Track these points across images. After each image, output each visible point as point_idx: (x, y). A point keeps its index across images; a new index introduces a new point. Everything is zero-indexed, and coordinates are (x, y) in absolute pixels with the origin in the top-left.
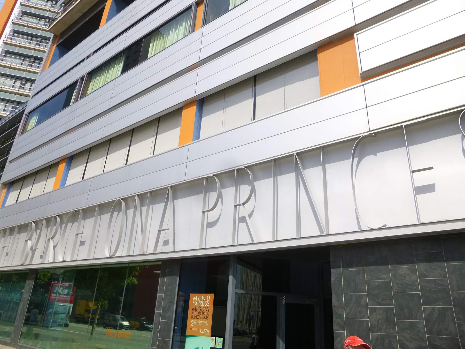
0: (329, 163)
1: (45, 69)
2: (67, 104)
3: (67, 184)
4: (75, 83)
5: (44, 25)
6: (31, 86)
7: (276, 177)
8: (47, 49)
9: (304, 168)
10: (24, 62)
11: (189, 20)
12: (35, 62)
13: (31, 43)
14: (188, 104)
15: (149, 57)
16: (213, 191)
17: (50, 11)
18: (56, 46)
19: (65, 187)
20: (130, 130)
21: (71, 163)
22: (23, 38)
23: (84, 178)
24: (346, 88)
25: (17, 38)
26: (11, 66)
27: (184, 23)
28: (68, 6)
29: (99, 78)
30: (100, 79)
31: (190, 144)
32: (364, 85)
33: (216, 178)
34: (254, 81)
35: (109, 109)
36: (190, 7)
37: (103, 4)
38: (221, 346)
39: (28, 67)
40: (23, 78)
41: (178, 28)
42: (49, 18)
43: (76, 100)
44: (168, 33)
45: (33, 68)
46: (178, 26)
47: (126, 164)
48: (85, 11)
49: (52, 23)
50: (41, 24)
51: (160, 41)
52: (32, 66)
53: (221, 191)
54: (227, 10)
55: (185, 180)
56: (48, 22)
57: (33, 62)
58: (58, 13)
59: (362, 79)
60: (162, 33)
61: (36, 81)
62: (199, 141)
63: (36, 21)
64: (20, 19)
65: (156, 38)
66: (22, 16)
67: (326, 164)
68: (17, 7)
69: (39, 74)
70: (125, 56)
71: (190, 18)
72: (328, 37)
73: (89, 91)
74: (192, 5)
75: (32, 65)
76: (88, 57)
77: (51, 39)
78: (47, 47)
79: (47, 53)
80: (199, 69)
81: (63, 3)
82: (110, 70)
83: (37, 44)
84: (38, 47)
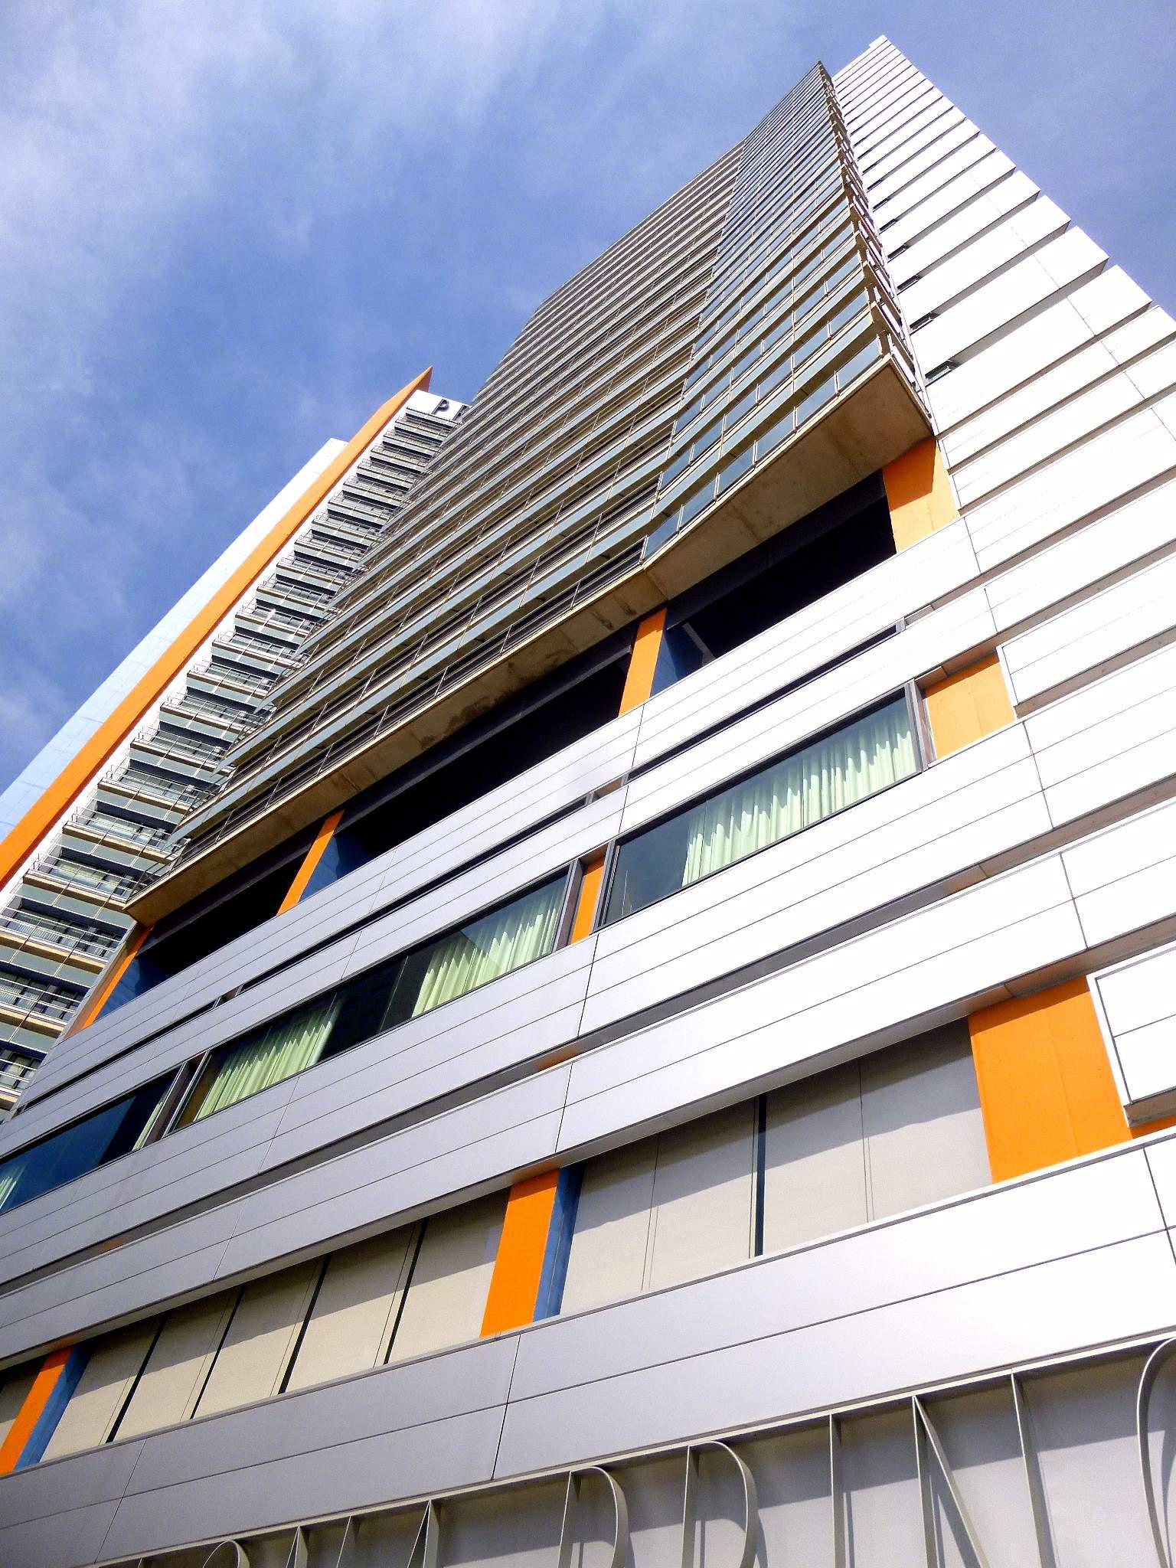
0: (1050, 1446)
1: (83, 1025)
2: (121, 1145)
3: (47, 1456)
4: (167, 1078)
5: (114, 892)
6: (23, 1075)
7: (845, 1495)
8: (104, 964)
9: (955, 1464)
10: (23, 997)
11: (554, 910)
12: (56, 999)
13: (63, 941)
14: (528, 1179)
15: (417, 1011)
16: (599, 1538)
17: (143, 855)
18: (136, 958)
19: (38, 1465)
20: (317, 1259)
21: (81, 1374)
22: (42, 925)
23: (117, 1438)
24: (1080, 1153)
25: (24, 924)
26: (28, 943)
27: (539, 918)
28: (199, 847)
29: (246, 1068)
30: (249, 1069)
31: (523, 1332)
32: (1143, 1146)
33: (612, 1482)
34: (757, 1117)
35: (260, 1175)
36: (561, 873)
37: (302, 847)
38: (844, 345)
39: (74, 951)
40: (93, 923)
41: (519, 932)
42: (136, 874)
43: (157, 1136)
44: (480, 956)
45: (48, 1018)
46: (518, 927)
47: (282, 1390)
48: (243, 863)
49: (141, 888)
50: (107, 889)
51: (458, 966)
52: (44, 1010)
53: (629, 1538)
54: (677, 888)
55: (492, 1480)
56: (130, 886)
57: (51, 999)
58: (166, 862)
59: (1134, 1125)
60: (467, 938)
61: (44, 1062)
62: (558, 1322)
63: (95, 880)
64: (50, 871)
65: (449, 953)
66: (57, 863)
67: (1039, 1451)
68: (52, 838)
69: (60, 1039)
70: (340, 1003)
71: (559, 903)
72: (1001, 983)
73: (204, 1110)
74: (568, 867)
75: (47, 1007)
76: (225, 999)
77: (126, 936)
78: (106, 954)
79: (102, 973)
80: (574, 1061)
81: (186, 837)
82: (288, 1043)
83: (78, 945)
84: (79, 956)
